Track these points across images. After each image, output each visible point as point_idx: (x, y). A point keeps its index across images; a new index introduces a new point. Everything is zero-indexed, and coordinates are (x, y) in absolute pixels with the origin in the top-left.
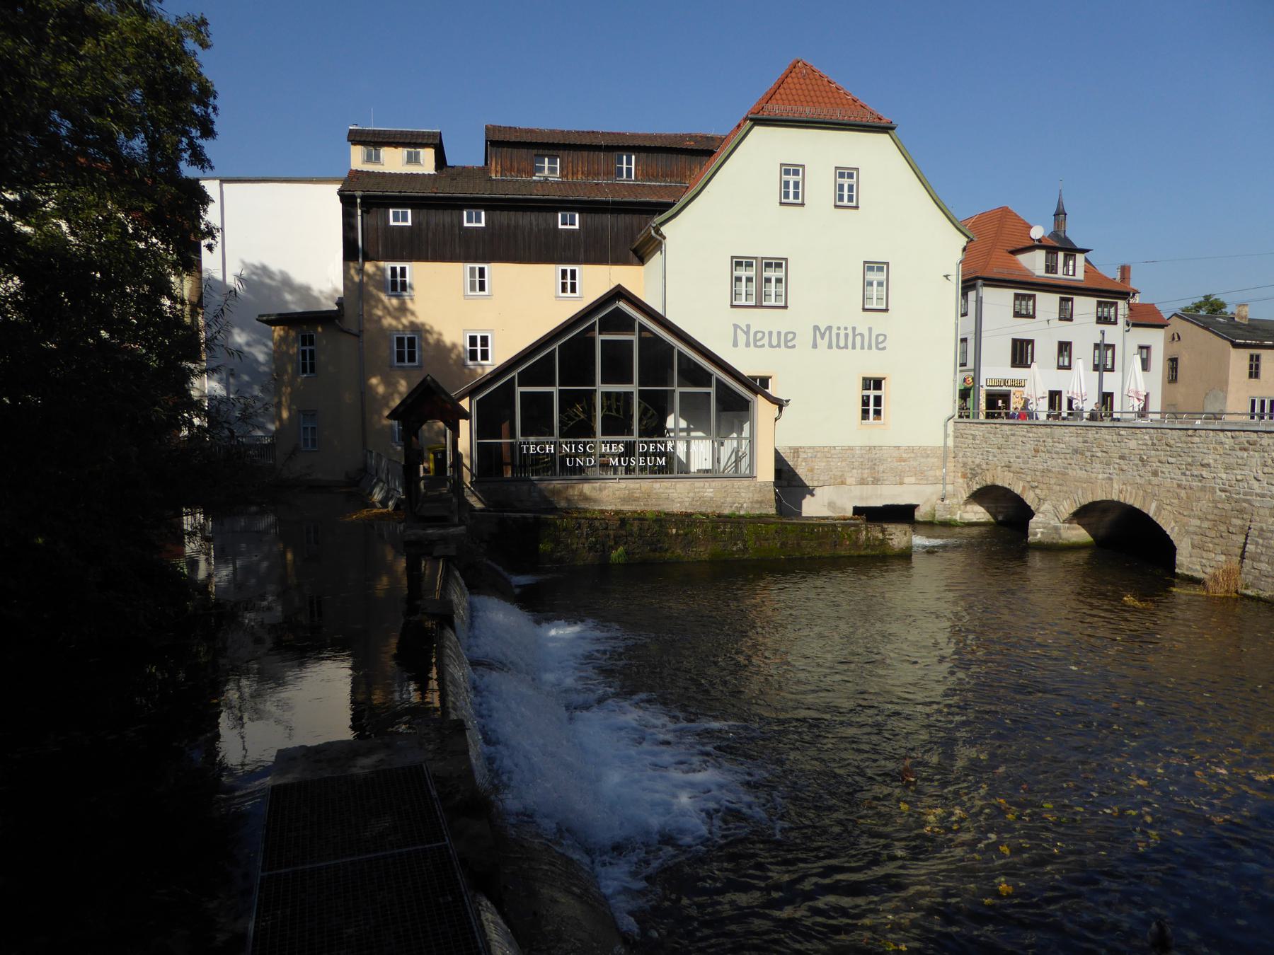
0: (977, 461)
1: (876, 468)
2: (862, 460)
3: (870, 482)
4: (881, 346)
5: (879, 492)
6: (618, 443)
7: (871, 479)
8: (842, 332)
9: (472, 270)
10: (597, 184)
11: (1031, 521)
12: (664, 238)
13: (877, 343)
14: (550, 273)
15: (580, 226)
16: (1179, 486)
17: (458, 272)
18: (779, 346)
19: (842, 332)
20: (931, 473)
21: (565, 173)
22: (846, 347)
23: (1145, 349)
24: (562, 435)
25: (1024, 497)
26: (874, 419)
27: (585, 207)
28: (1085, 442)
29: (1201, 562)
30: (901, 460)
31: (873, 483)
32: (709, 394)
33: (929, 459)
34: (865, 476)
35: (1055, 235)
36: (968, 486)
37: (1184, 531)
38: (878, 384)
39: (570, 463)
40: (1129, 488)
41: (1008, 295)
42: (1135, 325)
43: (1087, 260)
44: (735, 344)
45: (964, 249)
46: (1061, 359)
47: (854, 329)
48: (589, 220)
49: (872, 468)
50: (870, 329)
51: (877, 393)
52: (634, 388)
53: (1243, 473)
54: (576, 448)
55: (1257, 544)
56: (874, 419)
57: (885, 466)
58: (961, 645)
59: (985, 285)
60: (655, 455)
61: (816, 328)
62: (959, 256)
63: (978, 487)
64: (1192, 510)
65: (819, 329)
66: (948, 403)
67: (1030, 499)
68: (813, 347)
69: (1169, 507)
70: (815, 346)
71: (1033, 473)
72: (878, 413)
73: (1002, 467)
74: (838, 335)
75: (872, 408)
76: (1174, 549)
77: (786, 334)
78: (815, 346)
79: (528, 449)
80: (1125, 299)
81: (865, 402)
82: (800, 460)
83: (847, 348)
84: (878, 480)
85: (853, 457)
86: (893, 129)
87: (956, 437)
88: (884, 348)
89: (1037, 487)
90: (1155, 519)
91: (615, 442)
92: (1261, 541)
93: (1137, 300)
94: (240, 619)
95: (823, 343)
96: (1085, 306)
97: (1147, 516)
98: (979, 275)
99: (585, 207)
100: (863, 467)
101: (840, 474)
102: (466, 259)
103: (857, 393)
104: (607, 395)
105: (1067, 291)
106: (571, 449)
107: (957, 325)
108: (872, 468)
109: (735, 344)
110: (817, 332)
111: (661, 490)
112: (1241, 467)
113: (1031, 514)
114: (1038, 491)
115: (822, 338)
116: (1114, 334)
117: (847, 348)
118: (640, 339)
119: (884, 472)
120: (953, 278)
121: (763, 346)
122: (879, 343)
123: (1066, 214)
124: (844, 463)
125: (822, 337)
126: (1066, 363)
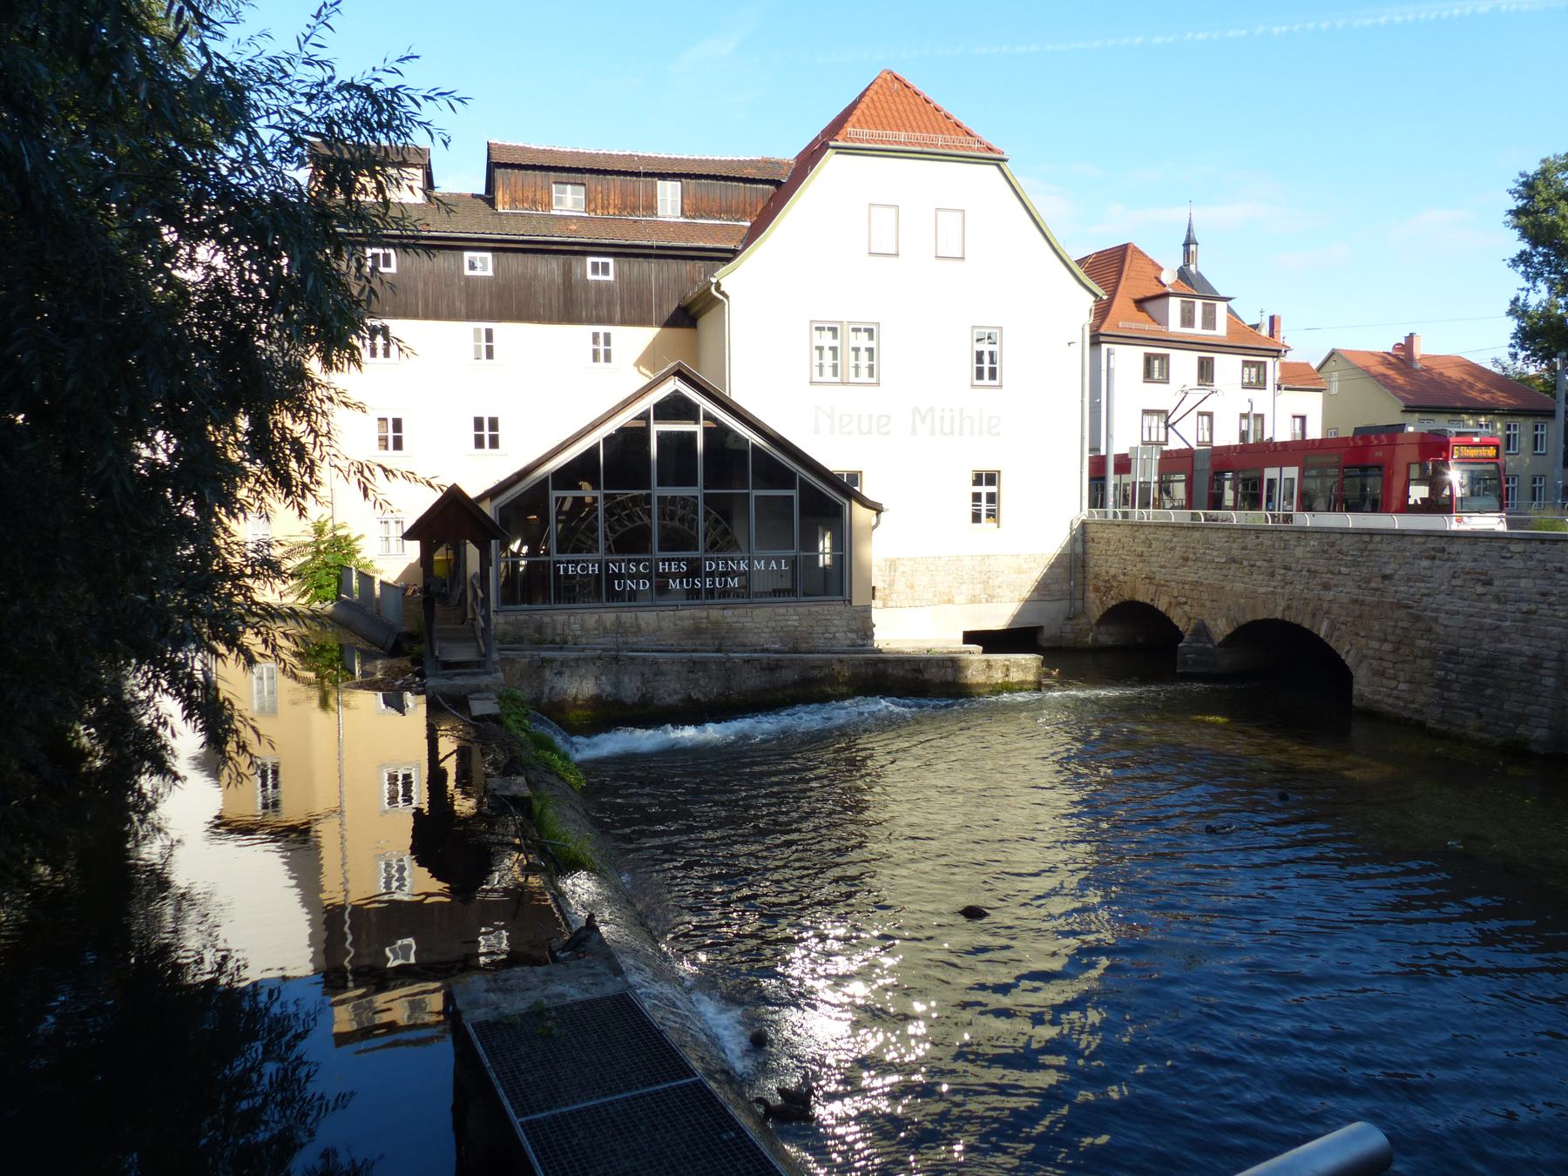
0: (1113, 571)
6: (679, 560)
9: (477, 331)
10: (635, 221)
12: (727, 297)
14: (578, 336)
15: (615, 277)
17: (463, 333)
18: (870, 432)
21: (592, 206)
24: (609, 550)
27: (621, 252)
28: (1244, 548)
31: (987, 601)
32: (791, 498)
34: (977, 592)
36: (1102, 602)
38: (991, 479)
39: (619, 586)
43: (1230, 310)
44: (817, 431)
48: (626, 268)
49: (986, 583)
51: (992, 489)
52: (697, 491)
54: (628, 568)
60: (724, 574)
61: (916, 410)
63: (1114, 603)
70: (914, 432)
71: (1180, 586)
77: (879, 417)
78: (914, 432)
79: (566, 569)
88: (998, 434)
89: (1185, 603)
90: (1327, 640)
91: (673, 560)
93: (1290, 358)
94: (75, 745)
96: (1228, 367)
97: (1338, 656)
99: (621, 252)
102: (470, 317)
104: (662, 500)
106: (620, 569)
108: (986, 583)
109: (817, 431)
111: (734, 619)
114: (1187, 608)
115: (923, 422)
118: (706, 430)
121: (851, 433)
125: (923, 419)
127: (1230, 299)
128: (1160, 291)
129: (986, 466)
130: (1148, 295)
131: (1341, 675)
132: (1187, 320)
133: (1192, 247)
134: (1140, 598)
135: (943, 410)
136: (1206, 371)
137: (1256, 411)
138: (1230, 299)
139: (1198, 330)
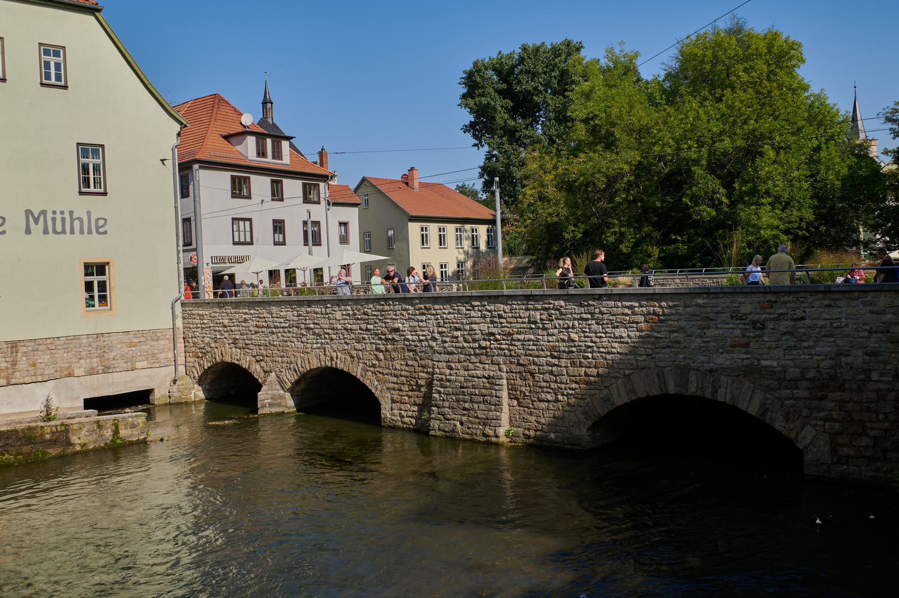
0: (207, 340)
1: (106, 355)
2: (90, 349)
3: (101, 371)
4: (101, 230)
5: (111, 381)
7: (100, 368)
8: (58, 217)
11: (259, 393)
12: (348, 186)
13: (97, 228)
16: (378, 350)
19: (58, 217)
20: (162, 356)
22: (64, 232)
23: (344, 224)
25: (252, 370)
26: (99, 306)
29: (400, 414)
30: (131, 345)
33: (160, 342)
34: (95, 365)
35: (263, 122)
37: (385, 388)
38: (101, 269)
40: (339, 354)
41: (224, 178)
42: (335, 204)
43: (292, 146)
45: (179, 135)
46: (276, 236)
47: (71, 213)
50: (89, 213)
51: (101, 278)
53: (424, 333)
55: (439, 392)
56: (99, 306)
57: (114, 353)
58: (196, 532)
59: (201, 167)
61: (28, 212)
62: (174, 141)
64: (389, 369)
65: (32, 214)
66: (175, 288)
67: (256, 370)
68: (44, 233)
69: (372, 369)
70: (28, 231)
72: (103, 299)
73: (229, 344)
74: (54, 220)
75: (96, 294)
76: (380, 404)
78: (28, 231)
80: (325, 181)
81: (89, 286)
82: (19, 354)
83: (65, 233)
84: (109, 368)
85: (80, 347)
86: (99, 11)
87: (184, 318)
88: (105, 233)
89: (261, 360)
90: (361, 379)
92: (442, 390)
93: (333, 183)
95: (37, 229)
96: (293, 188)
97: (355, 378)
98: (198, 157)
100: (92, 356)
101: (66, 365)
103: (80, 279)
105: (277, 175)
107: (176, 207)
110: (30, 217)
112: (422, 329)
113: (259, 387)
114: (263, 363)
116: (318, 212)
117: (65, 233)
119: (114, 359)
120: (169, 163)
122: (100, 228)
123: (272, 103)
124: (70, 354)
125: (36, 221)
126: (281, 240)
127: (291, 138)
128: (241, 129)
129: (97, 258)
130: (232, 132)
131: (375, 404)
132: (261, 153)
133: (269, 105)
134: (228, 359)
135: (54, 212)
136: (277, 194)
137: (313, 219)
138: (291, 138)
139: (269, 160)
